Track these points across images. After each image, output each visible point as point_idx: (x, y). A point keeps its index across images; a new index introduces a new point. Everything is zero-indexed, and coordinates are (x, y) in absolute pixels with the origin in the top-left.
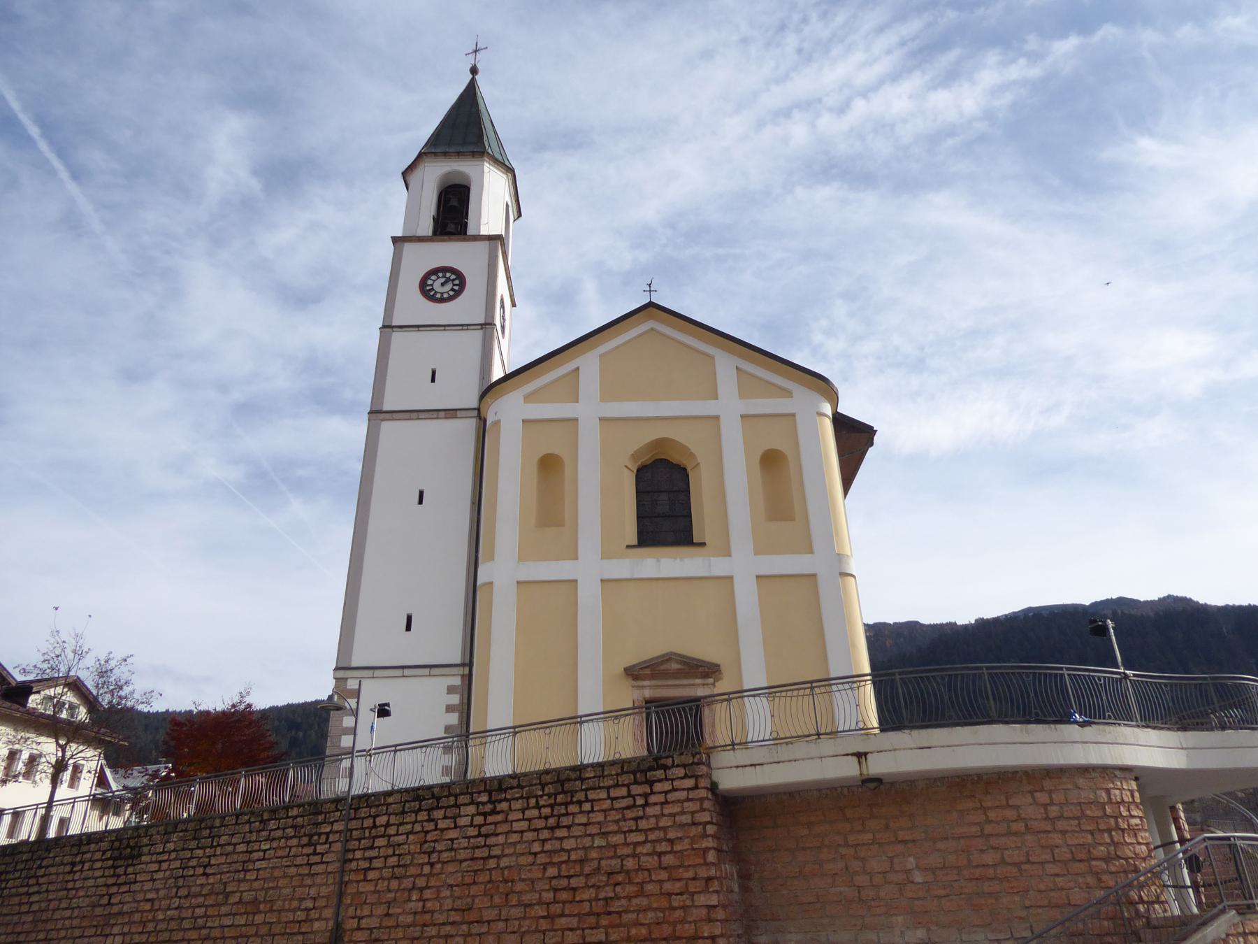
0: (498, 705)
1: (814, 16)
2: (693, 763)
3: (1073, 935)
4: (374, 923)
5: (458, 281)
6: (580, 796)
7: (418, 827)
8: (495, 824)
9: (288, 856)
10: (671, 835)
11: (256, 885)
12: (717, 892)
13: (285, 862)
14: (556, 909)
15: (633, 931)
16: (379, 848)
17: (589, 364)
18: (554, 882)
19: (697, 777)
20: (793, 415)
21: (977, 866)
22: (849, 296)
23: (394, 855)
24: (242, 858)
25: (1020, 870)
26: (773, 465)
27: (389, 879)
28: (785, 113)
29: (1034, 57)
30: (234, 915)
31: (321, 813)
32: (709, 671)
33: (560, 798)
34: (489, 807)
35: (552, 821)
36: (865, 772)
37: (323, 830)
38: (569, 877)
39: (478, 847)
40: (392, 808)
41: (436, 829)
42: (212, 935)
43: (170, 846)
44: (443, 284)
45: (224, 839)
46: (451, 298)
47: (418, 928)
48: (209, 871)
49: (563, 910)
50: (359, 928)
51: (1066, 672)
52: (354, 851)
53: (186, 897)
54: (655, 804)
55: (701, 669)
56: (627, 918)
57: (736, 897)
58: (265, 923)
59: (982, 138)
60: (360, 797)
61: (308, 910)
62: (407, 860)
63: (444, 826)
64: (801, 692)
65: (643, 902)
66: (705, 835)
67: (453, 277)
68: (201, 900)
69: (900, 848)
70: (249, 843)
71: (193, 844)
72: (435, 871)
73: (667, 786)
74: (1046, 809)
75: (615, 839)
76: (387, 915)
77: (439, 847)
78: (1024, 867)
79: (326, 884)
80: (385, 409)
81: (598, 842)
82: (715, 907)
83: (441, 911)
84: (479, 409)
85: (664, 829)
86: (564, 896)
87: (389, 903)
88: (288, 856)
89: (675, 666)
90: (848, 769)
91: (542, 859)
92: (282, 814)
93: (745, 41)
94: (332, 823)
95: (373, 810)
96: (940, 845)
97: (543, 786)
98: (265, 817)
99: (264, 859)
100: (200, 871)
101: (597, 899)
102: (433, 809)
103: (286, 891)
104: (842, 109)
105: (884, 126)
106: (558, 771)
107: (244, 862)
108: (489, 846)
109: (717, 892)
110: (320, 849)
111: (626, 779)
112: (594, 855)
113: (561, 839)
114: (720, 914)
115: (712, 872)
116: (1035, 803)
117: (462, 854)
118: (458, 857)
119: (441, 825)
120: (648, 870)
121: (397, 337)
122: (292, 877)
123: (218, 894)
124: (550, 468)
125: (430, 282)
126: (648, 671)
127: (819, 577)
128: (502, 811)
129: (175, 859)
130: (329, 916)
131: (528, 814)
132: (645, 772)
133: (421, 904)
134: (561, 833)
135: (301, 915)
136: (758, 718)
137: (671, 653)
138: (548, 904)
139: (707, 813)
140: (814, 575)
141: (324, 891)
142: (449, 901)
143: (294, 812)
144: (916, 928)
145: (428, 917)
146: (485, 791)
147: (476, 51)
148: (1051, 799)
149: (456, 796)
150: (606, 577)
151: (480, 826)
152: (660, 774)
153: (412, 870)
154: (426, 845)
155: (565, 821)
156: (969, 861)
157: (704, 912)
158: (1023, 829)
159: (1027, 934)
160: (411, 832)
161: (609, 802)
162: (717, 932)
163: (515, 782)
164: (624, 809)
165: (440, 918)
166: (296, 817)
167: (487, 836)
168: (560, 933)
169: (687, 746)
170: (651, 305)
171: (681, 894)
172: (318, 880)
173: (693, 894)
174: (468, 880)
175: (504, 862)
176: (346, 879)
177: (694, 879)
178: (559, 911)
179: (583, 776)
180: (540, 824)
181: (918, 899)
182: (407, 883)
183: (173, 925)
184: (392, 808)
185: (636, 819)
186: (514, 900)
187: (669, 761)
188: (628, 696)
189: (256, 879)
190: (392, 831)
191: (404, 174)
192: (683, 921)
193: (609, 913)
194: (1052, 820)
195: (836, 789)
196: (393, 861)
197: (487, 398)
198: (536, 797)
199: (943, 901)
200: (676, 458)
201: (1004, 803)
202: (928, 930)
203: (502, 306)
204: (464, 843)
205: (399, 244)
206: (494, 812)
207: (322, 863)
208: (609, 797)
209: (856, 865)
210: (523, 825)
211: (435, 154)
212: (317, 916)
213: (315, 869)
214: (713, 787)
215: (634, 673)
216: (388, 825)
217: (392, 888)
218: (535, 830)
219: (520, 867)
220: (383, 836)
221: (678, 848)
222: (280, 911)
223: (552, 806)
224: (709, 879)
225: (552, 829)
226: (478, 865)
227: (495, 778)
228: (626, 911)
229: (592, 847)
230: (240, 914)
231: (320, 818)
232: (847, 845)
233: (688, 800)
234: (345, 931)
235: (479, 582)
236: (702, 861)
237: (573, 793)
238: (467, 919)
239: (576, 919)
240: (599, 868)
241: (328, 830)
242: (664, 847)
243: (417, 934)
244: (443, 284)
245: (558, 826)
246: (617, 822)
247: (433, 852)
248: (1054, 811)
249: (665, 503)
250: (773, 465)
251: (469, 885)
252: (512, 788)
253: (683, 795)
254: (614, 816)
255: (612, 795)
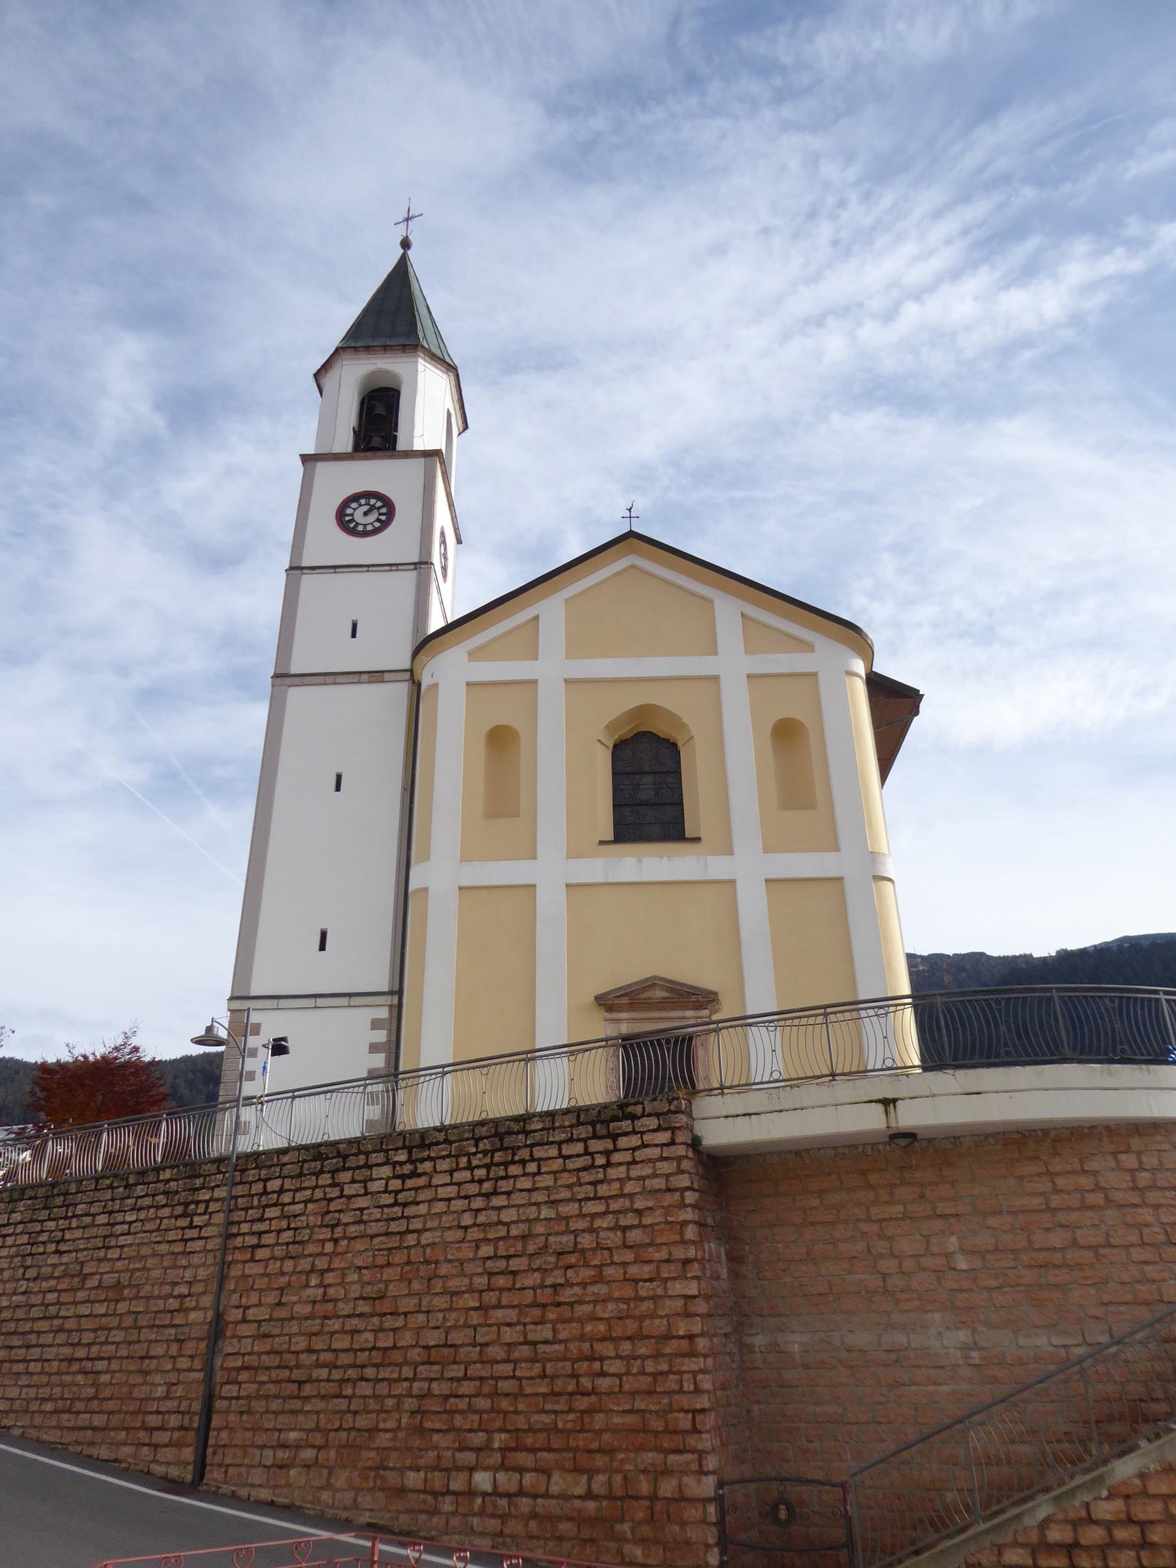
0: (434, 1039)
1: (853, 197)
2: (669, 1111)
3: (1166, 1341)
4: (263, 1313)
5: (383, 509)
6: (524, 1154)
7: (319, 1194)
8: (416, 1189)
9: (158, 1230)
10: (639, 1204)
11: (119, 1265)
12: (698, 1278)
13: (155, 1237)
14: (491, 1298)
15: (589, 1328)
16: (271, 1219)
17: (551, 611)
18: (489, 1263)
19: (673, 1130)
20: (815, 675)
21: (1041, 1249)
22: (899, 550)
23: (289, 1228)
24: (102, 1231)
25: (1097, 1255)
26: (789, 737)
27: (282, 1259)
28: (818, 321)
29: (1136, 245)
30: (93, 1302)
31: (199, 1176)
32: (704, 999)
33: (498, 1157)
34: (407, 1169)
35: (487, 1186)
36: (893, 1124)
37: (201, 1198)
38: (508, 1258)
39: (393, 1219)
40: (287, 1170)
41: (342, 1196)
42: (66, 1326)
43: (17, 1217)
44: (366, 514)
45: (80, 1209)
46: (376, 531)
47: (318, 1321)
48: (63, 1247)
49: (499, 1300)
50: (244, 1321)
51: (1162, 997)
52: (239, 1223)
53: (35, 1279)
54: (620, 1164)
55: (693, 998)
56: (583, 1310)
57: (724, 1285)
58: (129, 1312)
59: (1068, 350)
60: (247, 1156)
61: (182, 1297)
62: (305, 1235)
63: (353, 1192)
64: (812, 1020)
65: (602, 1289)
66: (682, 1205)
67: (379, 504)
68: (53, 1283)
69: (939, 1224)
70: (110, 1213)
71: (44, 1214)
72: (339, 1249)
73: (635, 1141)
74: (1133, 1176)
75: (571, 1209)
76: (279, 1304)
77: (345, 1219)
78: (1102, 1251)
79: (204, 1265)
80: (293, 671)
81: (546, 1212)
82: (694, 1297)
83: (346, 1299)
84: (411, 671)
85: (631, 1196)
86: (501, 1281)
87: (282, 1289)
88: (158, 1230)
89: (660, 994)
90: (872, 1120)
91: (474, 1234)
92: (152, 1177)
93: (766, 231)
94: (213, 1188)
95: (263, 1172)
96: (991, 1221)
97: (477, 1141)
98: (131, 1181)
99: (129, 1233)
100: (52, 1247)
101: (543, 1286)
102: (338, 1170)
103: (156, 1273)
104: (890, 315)
105: (942, 337)
106: (496, 1122)
107: (105, 1237)
108: (408, 1218)
109: (698, 1278)
110: (197, 1221)
111: (583, 1131)
112: (540, 1229)
113: (499, 1209)
114: (702, 1307)
115: (691, 1252)
116: (1119, 1167)
117: (374, 1228)
118: (369, 1232)
119: (348, 1190)
120: (608, 1249)
121: (307, 580)
122: (162, 1256)
123: (73, 1276)
124: (502, 743)
125: (349, 511)
126: (625, 1000)
127: (846, 881)
128: (425, 1174)
129: (22, 1233)
130: (208, 1305)
131: (459, 1176)
132: (606, 1122)
133: (321, 1290)
134: (497, 1201)
135: (173, 1304)
136: (765, 1054)
137: (655, 977)
138: (481, 1292)
139: (686, 1176)
140: (840, 879)
141: (202, 1273)
142: (357, 1287)
143: (167, 1175)
144: (958, 1329)
145: (330, 1306)
146: (404, 1147)
147: (407, 219)
148: (1140, 1162)
149: (367, 1154)
150: (572, 881)
151: (397, 1192)
152: (626, 1125)
153: (311, 1248)
154: (329, 1217)
155: (504, 1186)
156: (1030, 1241)
157: (680, 1303)
158: (1102, 1202)
159: (1104, 1339)
160: (311, 1200)
161: (560, 1161)
162: (697, 1329)
163: (441, 1137)
164: (579, 1170)
165: (345, 1308)
166: (169, 1181)
167: (405, 1205)
168: (495, 1328)
169: (662, 1089)
170: (631, 535)
171: (651, 1280)
172: (195, 1259)
173: (666, 1280)
174: (380, 1261)
175: (427, 1238)
176: (229, 1258)
177: (667, 1261)
178: (494, 1301)
179: (528, 1128)
180: (473, 1189)
181: (962, 1291)
182: (304, 1264)
183: (20, 1314)
184: (287, 1170)
185: (594, 1184)
186: (438, 1286)
187: (638, 1110)
188: (599, 1027)
189: (120, 1258)
190: (286, 1198)
191: (317, 376)
192: (652, 1315)
193: (559, 1304)
194: (1141, 1191)
195: (855, 1146)
196: (287, 1236)
197: (421, 656)
198: (468, 1155)
199: (995, 1294)
200: (662, 729)
201: (1077, 1166)
202: (974, 1331)
203: (443, 542)
204: (377, 1214)
205: (308, 464)
206: (414, 1174)
207: (200, 1238)
208: (560, 1156)
209: (880, 1246)
210: (451, 1191)
211: (356, 349)
212: (193, 1304)
213: (191, 1246)
214: (695, 1143)
215: (607, 1003)
216: (281, 1191)
217: (285, 1269)
218: (466, 1197)
219: (446, 1244)
220: (275, 1205)
221: (647, 1221)
222: (148, 1298)
223: (488, 1167)
224: (687, 1262)
225: (487, 1196)
226: (394, 1242)
227: (416, 1131)
228: (581, 1302)
229: (537, 1219)
230: (100, 1301)
231: (198, 1182)
232: (869, 1219)
233: (662, 1159)
234: (228, 1323)
235: (411, 888)
236: (677, 1238)
237: (514, 1150)
238: (378, 1310)
239: (516, 1311)
240: (546, 1246)
241: (207, 1197)
242: (629, 1220)
243: (316, 1329)
244: (366, 514)
245: (495, 1193)
246: (570, 1187)
247: (337, 1225)
248: (1144, 1178)
249: (648, 789)
250: (789, 737)
251: (382, 1267)
252: (438, 1143)
253: (654, 1152)
254: (567, 1179)
255: (565, 1152)
